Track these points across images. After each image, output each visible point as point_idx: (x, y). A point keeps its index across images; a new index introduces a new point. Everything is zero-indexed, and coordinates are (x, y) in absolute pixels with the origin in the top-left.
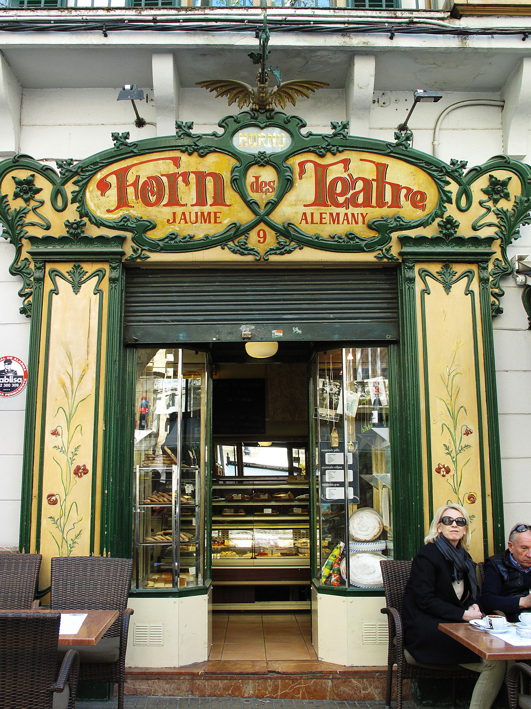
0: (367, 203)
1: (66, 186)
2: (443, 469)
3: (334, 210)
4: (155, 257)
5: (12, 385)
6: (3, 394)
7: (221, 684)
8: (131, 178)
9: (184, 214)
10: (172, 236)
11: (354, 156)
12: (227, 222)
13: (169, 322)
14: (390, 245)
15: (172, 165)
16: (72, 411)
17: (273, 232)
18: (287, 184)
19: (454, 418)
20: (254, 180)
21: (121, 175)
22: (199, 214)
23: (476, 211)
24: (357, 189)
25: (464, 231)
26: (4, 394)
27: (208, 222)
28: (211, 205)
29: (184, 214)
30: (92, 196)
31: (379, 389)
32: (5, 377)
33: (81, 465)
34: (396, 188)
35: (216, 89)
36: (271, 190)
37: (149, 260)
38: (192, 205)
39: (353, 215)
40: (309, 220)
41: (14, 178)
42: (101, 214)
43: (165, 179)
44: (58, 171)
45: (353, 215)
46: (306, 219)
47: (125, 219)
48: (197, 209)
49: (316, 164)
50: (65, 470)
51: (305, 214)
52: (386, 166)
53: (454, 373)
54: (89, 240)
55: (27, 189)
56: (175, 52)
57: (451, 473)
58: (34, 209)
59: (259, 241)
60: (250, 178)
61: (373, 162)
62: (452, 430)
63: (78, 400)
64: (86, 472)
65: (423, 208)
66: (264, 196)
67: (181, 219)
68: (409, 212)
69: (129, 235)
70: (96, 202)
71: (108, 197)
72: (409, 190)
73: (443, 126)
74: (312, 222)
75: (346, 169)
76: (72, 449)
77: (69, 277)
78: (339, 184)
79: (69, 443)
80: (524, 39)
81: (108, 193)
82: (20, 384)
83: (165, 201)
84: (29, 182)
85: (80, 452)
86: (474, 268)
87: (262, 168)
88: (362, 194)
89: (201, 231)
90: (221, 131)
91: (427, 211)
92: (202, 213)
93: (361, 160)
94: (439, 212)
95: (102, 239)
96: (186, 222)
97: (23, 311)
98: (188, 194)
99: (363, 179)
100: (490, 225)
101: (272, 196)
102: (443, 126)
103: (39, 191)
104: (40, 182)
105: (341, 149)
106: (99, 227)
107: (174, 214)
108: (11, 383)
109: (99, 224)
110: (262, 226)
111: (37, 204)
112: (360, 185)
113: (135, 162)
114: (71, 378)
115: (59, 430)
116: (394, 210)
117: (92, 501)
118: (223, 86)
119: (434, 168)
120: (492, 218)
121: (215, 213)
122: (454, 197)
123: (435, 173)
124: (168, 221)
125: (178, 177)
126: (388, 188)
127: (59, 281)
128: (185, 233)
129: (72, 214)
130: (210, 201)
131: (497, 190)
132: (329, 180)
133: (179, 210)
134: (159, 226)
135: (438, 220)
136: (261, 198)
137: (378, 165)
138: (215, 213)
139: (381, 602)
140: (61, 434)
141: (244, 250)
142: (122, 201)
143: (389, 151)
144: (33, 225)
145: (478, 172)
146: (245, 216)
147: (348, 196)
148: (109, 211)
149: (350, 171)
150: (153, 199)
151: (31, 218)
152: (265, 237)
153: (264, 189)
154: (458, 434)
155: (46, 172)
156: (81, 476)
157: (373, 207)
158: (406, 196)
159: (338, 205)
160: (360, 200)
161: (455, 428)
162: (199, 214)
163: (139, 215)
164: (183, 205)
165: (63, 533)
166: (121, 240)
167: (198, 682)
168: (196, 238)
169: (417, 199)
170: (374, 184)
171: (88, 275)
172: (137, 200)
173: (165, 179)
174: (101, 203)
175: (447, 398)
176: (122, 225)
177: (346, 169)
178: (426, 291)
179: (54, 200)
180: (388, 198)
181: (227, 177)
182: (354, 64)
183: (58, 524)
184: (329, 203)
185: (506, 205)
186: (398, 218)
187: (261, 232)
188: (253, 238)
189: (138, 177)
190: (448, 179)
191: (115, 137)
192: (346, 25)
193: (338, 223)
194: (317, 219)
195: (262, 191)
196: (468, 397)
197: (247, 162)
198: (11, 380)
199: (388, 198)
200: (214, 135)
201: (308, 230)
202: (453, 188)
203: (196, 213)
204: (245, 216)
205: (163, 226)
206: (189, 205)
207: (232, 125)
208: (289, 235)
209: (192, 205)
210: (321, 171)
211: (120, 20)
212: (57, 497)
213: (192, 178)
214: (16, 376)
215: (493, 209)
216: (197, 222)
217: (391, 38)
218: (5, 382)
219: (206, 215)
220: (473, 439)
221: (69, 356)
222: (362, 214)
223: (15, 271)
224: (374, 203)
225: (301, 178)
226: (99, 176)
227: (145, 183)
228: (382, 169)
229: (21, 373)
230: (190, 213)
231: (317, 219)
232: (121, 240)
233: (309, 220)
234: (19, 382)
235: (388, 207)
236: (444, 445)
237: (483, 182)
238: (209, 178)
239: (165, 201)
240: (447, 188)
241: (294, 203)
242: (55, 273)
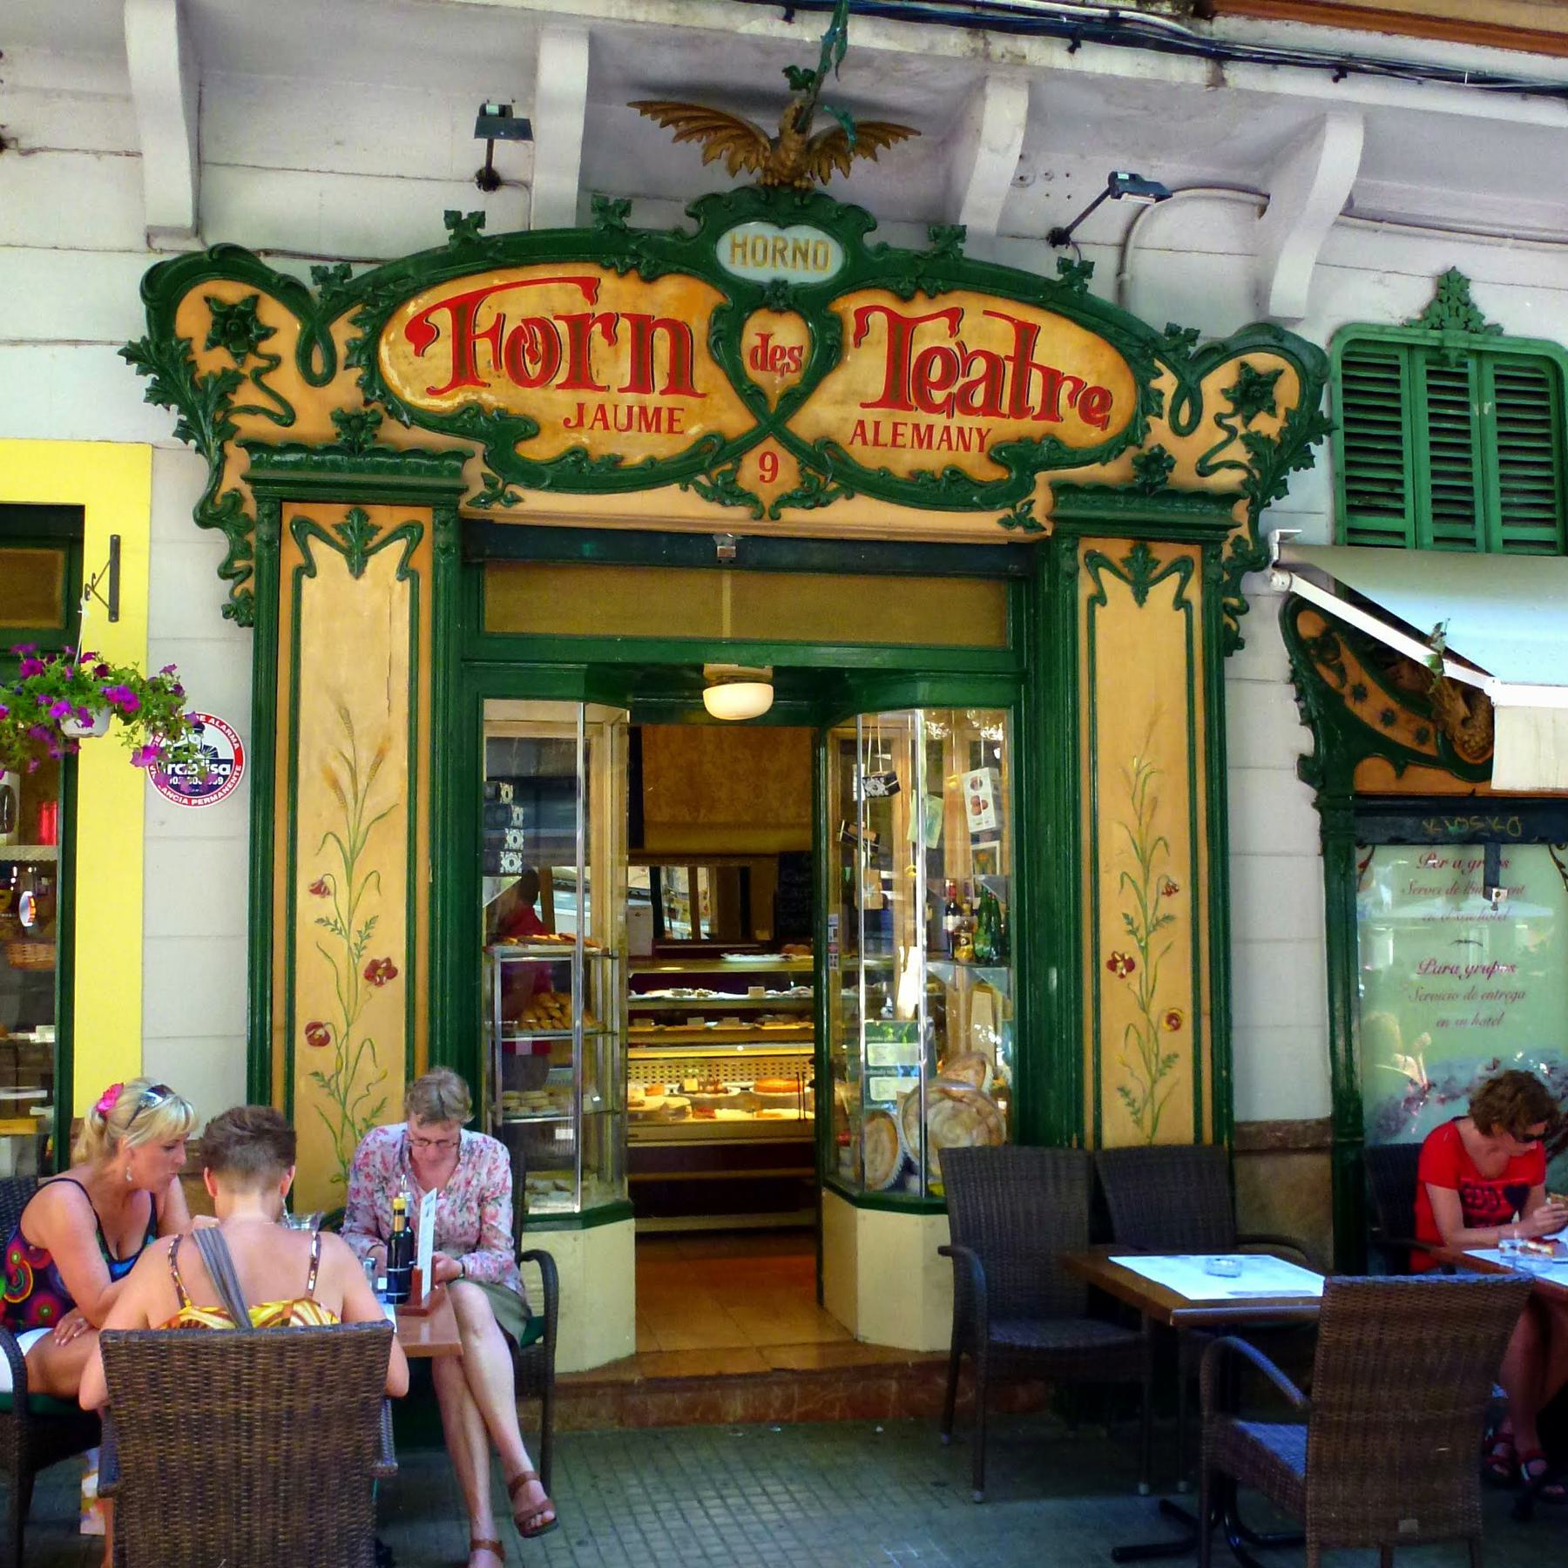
0: (991, 408)
2: (1120, 964)
3: (924, 418)
4: (539, 504)
7: (678, 1401)
8: (485, 318)
9: (601, 408)
11: (972, 305)
12: (694, 430)
14: (1031, 497)
15: (579, 296)
17: (793, 460)
19: (1145, 863)
20: (757, 341)
21: (464, 309)
22: (636, 409)
23: (1208, 434)
25: (1184, 475)
28: (663, 393)
29: (601, 408)
30: (394, 353)
31: (981, 798)
33: (380, 957)
34: (1053, 378)
35: (675, 122)
36: (793, 366)
37: (519, 507)
38: (621, 390)
39: (961, 431)
40: (870, 435)
41: (207, 300)
42: (412, 395)
43: (562, 327)
44: (314, 289)
45: (961, 431)
47: (466, 408)
48: (631, 398)
49: (893, 317)
50: (343, 972)
51: (861, 423)
53: (1147, 770)
55: (236, 328)
56: (1369, 117)
57: (1136, 972)
58: (258, 376)
59: (762, 477)
60: (750, 339)
62: (1140, 884)
63: (368, 816)
64: (391, 972)
65: (1104, 423)
66: (778, 379)
68: (1074, 429)
69: (479, 448)
70: (404, 368)
72: (1078, 383)
74: (876, 443)
75: (954, 329)
76: (358, 925)
77: (339, 538)
78: (937, 364)
79: (351, 912)
80: (1336, 80)
82: (225, 777)
83: (561, 377)
85: (378, 931)
86: (1193, 552)
87: (776, 317)
88: (982, 387)
89: (637, 448)
91: (1111, 430)
92: (643, 410)
94: (1132, 434)
96: (606, 427)
98: (613, 364)
100: (1233, 465)
101: (794, 378)
103: (268, 333)
104: (273, 312)
110: (771, 444)
111: (264, 363)
112: (979, 367)
113: (496, 282)
115: (329, 882)
116: (1043, 426)
117: (407, 1035)
118: (695, 118)
120: (1237, 452)
121: (671, 411)
122: (1167, 402)
124: (567, 421)
126: (1036, 378)
127: (318, 548)
128: (606, 450)
129: (345, 390)
130: (660, 381)
131: (1253, 393)
132: (917, 350)
133: (591, 398)
134: (546, 433)
135: (1131, 451)
136: (774, 383)
138: (671, 411)
139: (938, 1228)
141: (728, 493)
144: (252, 410)
145: (1219, 353)
146: (735, 419)
147: (955, 389)
149: (964, 335)
150: (534, 370)
151: (247, 395)
153: (779, 364)
154: (1151, 894)
155: (289, 291)
156: (381, 984)
157: (1004, 416)
159: (933, 408)
160: (978, 399)
161: (1146, 881)
162: (636, 409)
164: (602, 389)
165: (344, 1104)
166: (462, 456)
167: (633, 1400)
168: (627, 463)
169: (1093, 403)
171: (382, 534)
173: (562, 327)
174: (416, 373)
175: (1132, 821)
176: (462, 422)
177: (954, 329)
178: (1099, 598)
179: (304, 357)
181: (699, 328)
182: (985, 98)
183: (333, 1085)
184: (913, 402)
185: (1268, 425)
186: (1056, 443)
188: (750, 471)
189: (501, 319)
190: (1158, 364)
191: (453, 218)
192: (978, 10)
193: (930, 446)
194: (886, 435)
195: (773, 368)
196: (1173, 820)
197: (749, 298)
201: (866, 456)
202: (1167, 383)
203: (630, 408)
204: (735, 419)
205: (556, 433)
206: (614, 389)
207: (719, 213)
208: (829, 470)
209: (621, 390)
210: (902, 331)
212: (329, 1028)
213: (624, 328)
215: (1242, 431)
216: (629, 426)
217: (788, 18)
219: (650, 413)
220: (1180, 905)
221: (345, 715)
222: (979, 430)
223: (207, 516)
225: (858, 344)
226: (412, 309)
227: (518, 333)
228: (1026, 335)
229: (226, 752)
231: (886, 435)
233: (870, 435)
235: (1035, 418)
236: (1126, 916)
237: (1222, 378)
239: (561, 377)
240: (1156, 384)
242: (305, 529)
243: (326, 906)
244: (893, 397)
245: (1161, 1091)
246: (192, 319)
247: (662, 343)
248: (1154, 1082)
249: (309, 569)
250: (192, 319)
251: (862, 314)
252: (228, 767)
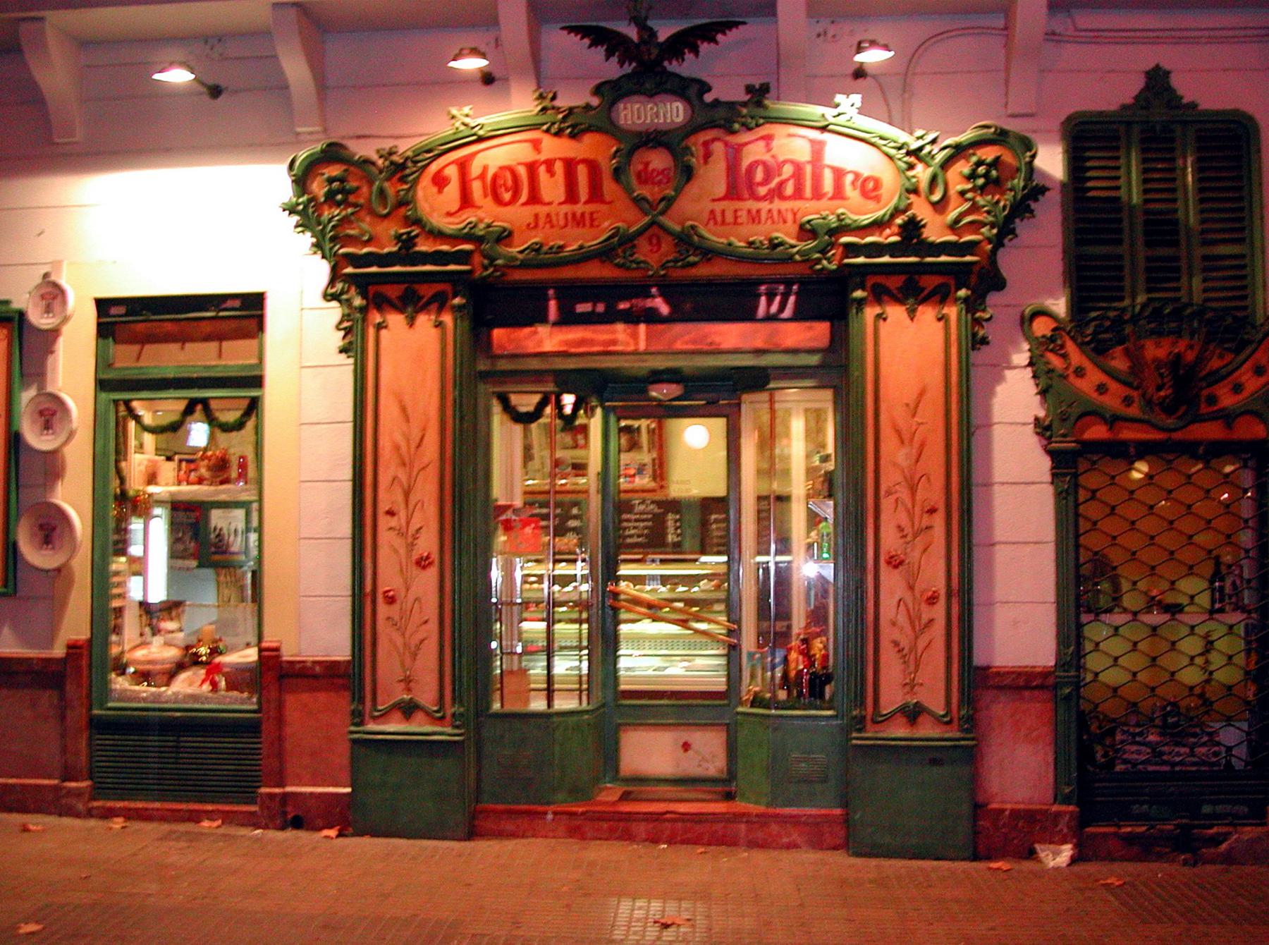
8: (475, 169)
10: (537, 249)
19: (913, 490)
24: (784, 177)
34: (839, 174)
42: (439, 221)
43: (522, 171)
45: (779, 212)
46: (714, 218)
49: (726, 144)
51: (712, 212)
65: (877, 199)
72: (857, 175)
73: (918, 70)
79: (408, 523)
81: (446, 189)
90: (595, 102)
92: (574, 215)
97: (343, 350)
99: (792, 162)
102: (918, 70)
105: (761, 121)
110: (655, 229)
112: (788, 170)
121: (592, 214)
133: (542, 210)
137: (812, 142)
142: (466, 200)
148: (449, 214)
149: (773, 152)
150: (507, 196)
160: (789, 190)
169: (870, 187)
177: (769, 149)
181: (607, 166)
194: (729, 218)
200: (588, 107)
211: (192, 387)
213: (559, 167)
216: (566, 226)
226: (434, 167)
227: (495, 177)
231: (729, 218)
233: (719, 218)
235: (831, 199)
239: (524, 197)
243: (393, 522)
244: (733, 193)
245: (921, 644)
246: (319, 188)
248: (916, 638)
251: (706, 144)
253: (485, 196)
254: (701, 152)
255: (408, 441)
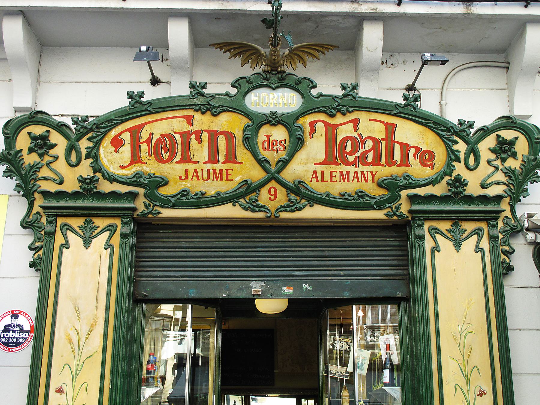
0: (376, 162)
1: (80, 142)
4: (167, 213)
5: (17, 340)
6: (8, 349)
8: (144, 136)
9: (196, 171)
11: (363, 117)
12: (238, 179)
13: (179, 277)
16: (78, 368)
18: (297, 143)
21: (135, 132)
22: (211, 171)
26: (9, 349)
27: (219, 179)
28: (223, 163)
29: (196, 171)
32: (11, 331)
37: (160, 216)
38: (204, 163)
39: (363, 173)
40: (320, 178)
43: (178, 137)
44: (73, 127)
45: (363, 173)
46: (316, 177)
48: (209, 166)
49: (326, 124)
51: (315, 172)
52: (395, 126)
53: (465, 332)
54: (101, 196)
61: (382, 122)
63: (84, 356)
65: (432, 166)
67: (193, 176)
71: (121, 153)
72: (417, 149)
75: (356, 128)
77: (80, 232)
82: (25, 339)
84: (44, 138)
92: (214, 171)
93: (370, 120)
95: (114, 195)
98: (200, 151)
106: (111, 183)
107: (187, 171)
108: (17, 338)
109: (112, 179)
112: (369, 144)
114: (78, 333)
119: (442, 128)
121: (227, 171)
123: (443, 133)
124: (181, 177)
125: (191, 135)
126: (397, 147)
130: (222, 158)
132: (339, 139)
137: (387, 125)
138: (227, 171)
140: (65, 392)
143: (397, 111)
145: (485, 132)
150: (166, 156)
152: (276, 194)
153: (275, 148)
155: (61, 128)
157: (383, 165)
158: (414, 155)
159: (348, 164)
160: (370, 158)
161: (468, 389)
162: (211, 171)
163: (152, 172)
169: (426, 157)
170: (384, 143)
172: (150, 156)
173: (178, 137)
174: (115, 160)
177: (356, 128)
180: (397, 156)
181: (239, 135)
187: (272, 190)
189: (152, 135)
193: (348, 181)
194: (327, 176)
198: (17, 335)
199: (397, 156)
203: (209, 170)
206: (201, 162)
207: (245, 85)
209: (204, 163)
214: (22, 331)
218: (11, 336)
219: (218, 172)
224: (383, 161)
226: (114, 133)
228: (391, 129)
230: (202, 170)
231: (327, 176)
232: (133, 196)
233: (320, 178)
234: (25, 337)
235: (397, 166)
238: (221, 137)
241: (304, 161)
244: (330, 160)
246: (23, 142)
247: (222, 142)
249: (66, 245)
250: (23, 142)
251: (312, 124)
252: (27, 334)
253: (150, 154)
254: (308, 129)
255: (79, 335)
